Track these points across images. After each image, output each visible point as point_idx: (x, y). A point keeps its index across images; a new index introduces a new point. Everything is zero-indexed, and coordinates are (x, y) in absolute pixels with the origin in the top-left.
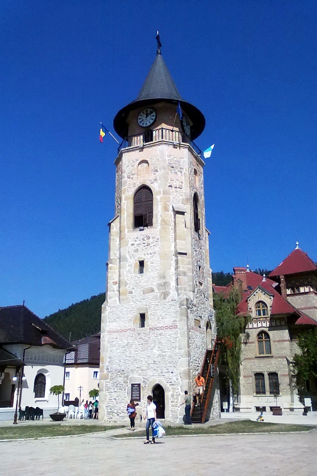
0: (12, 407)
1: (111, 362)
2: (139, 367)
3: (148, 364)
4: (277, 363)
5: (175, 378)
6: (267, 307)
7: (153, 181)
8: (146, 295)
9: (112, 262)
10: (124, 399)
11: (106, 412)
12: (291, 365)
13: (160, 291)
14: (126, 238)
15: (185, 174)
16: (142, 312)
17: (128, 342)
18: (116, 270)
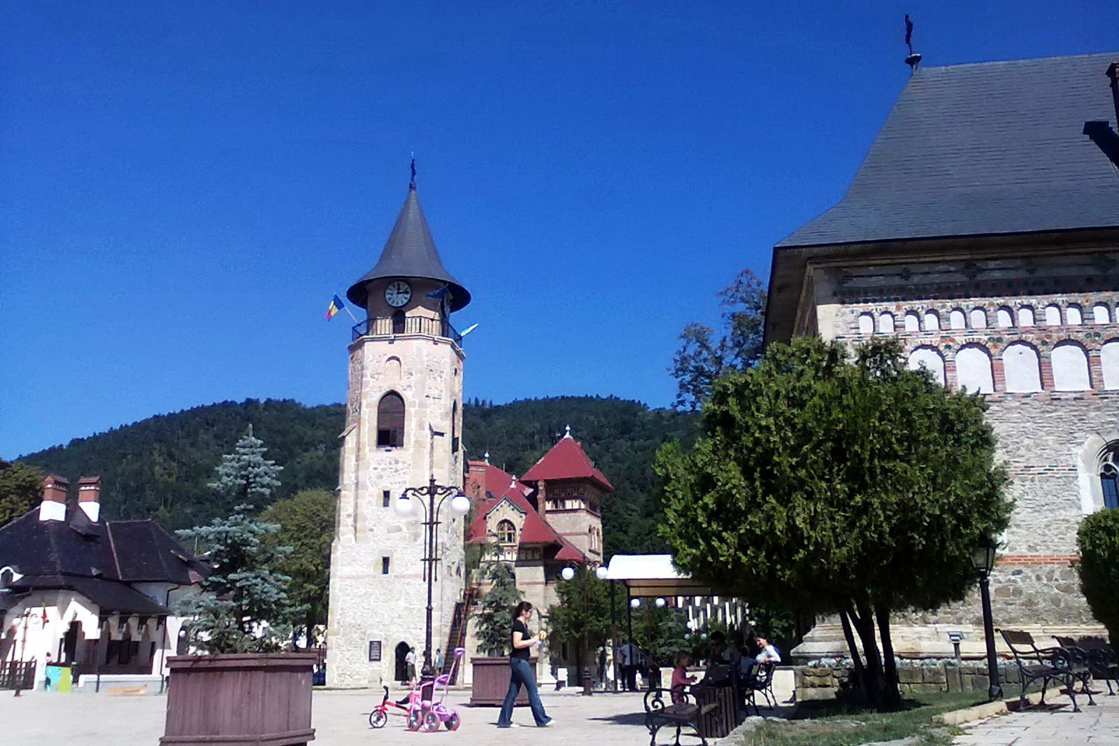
0: (151, 673)
6: (514, 529)
8: (392, 534)
12: (543, 620)
16: (385, 556)
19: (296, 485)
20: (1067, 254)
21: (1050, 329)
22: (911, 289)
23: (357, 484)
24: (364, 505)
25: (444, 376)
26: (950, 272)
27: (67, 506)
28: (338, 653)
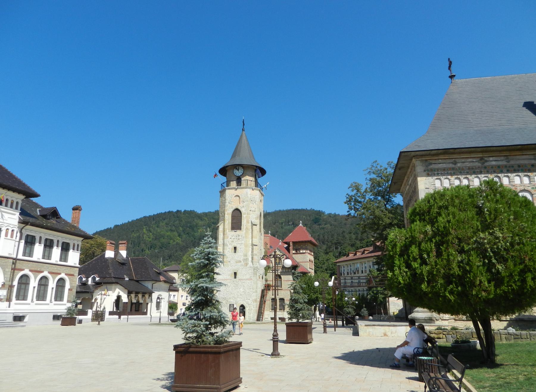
5: (250, 302)
16: (235, 272)
19: (195, 241)
20: (523, 155)
21: (517, 185)
22: (456, 169)
24: (227, 252)
25: (257, 203)
26: (473, 162)
27: (115, 252)
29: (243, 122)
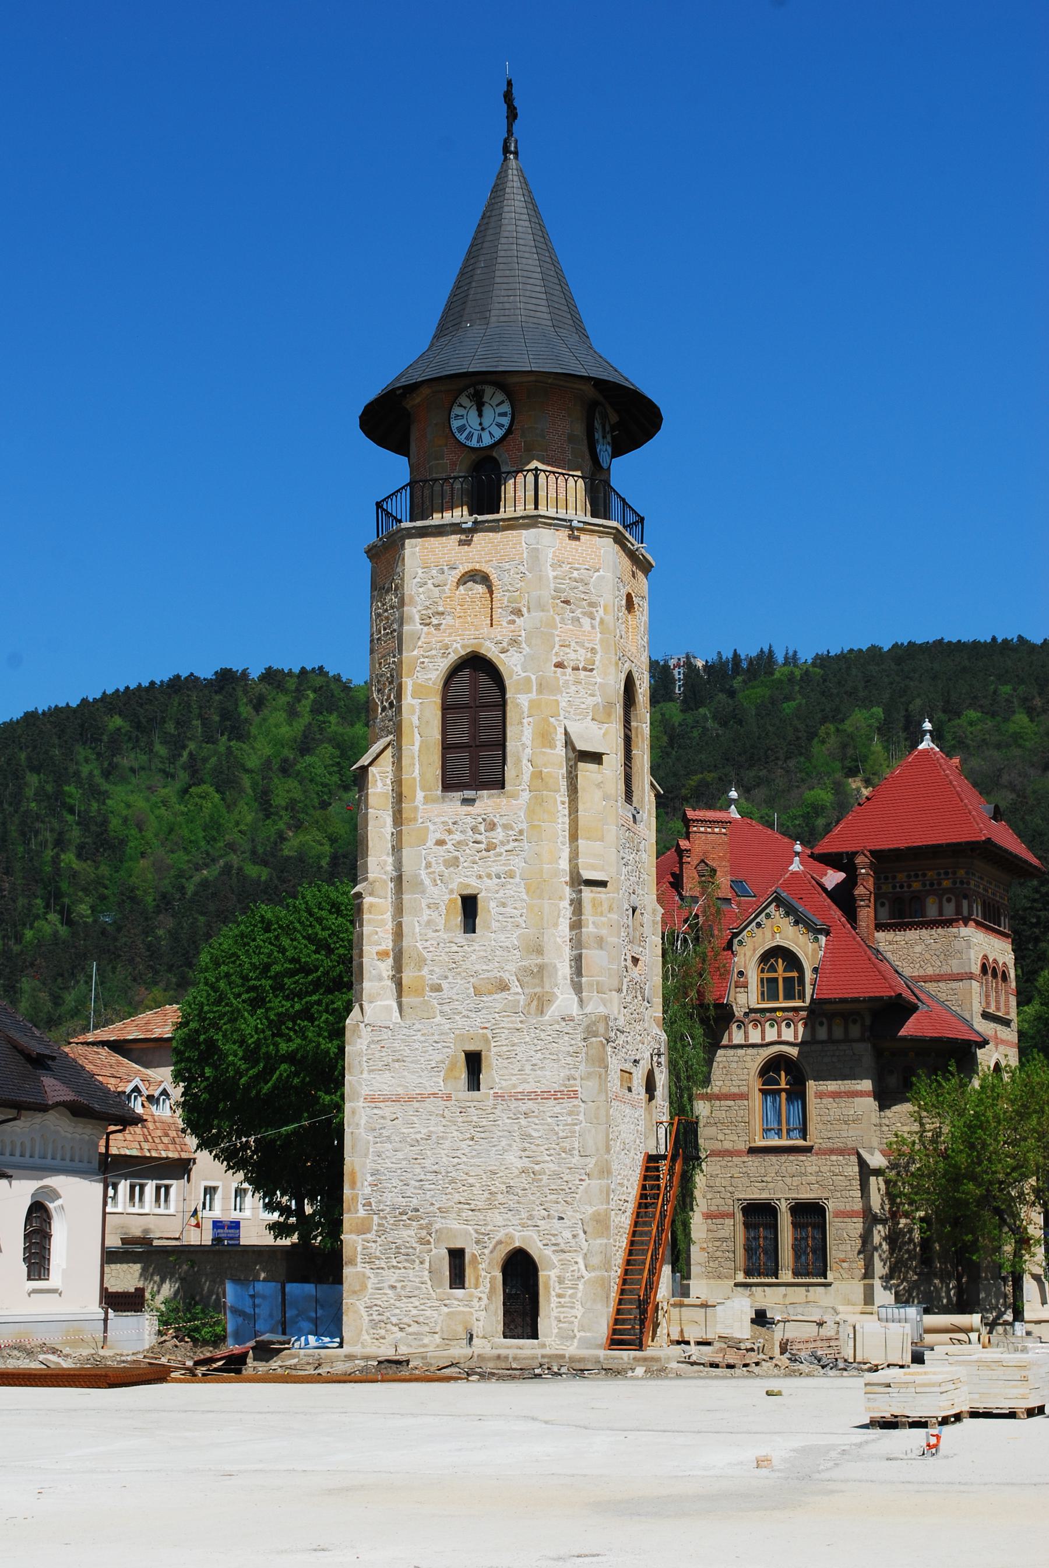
1: (380, 1186)
2: (462, 1200)
3: (490, 1193)
4: (824, 1169)
5: (567, 1234)
7: (505, 644)
9: (373, 890)
10: (419, 1288)
11: (366, 1321)
13: (527, 991)
14: (420, 821)
15: (602, 622)
17: (431, 1132)
18: (385, 916)
23: (398, 880)
28: (369, 1273)
29: (508, 97)
